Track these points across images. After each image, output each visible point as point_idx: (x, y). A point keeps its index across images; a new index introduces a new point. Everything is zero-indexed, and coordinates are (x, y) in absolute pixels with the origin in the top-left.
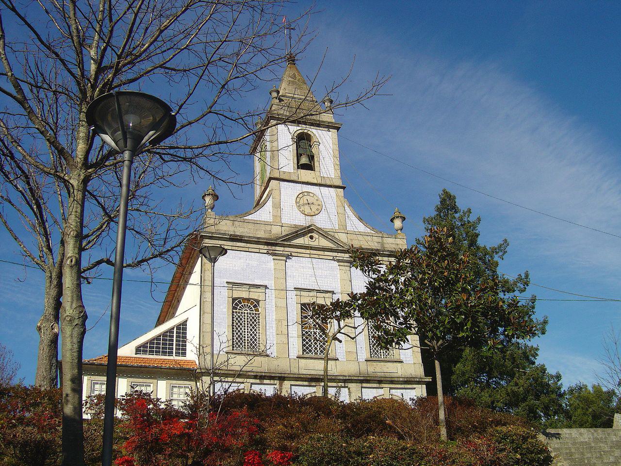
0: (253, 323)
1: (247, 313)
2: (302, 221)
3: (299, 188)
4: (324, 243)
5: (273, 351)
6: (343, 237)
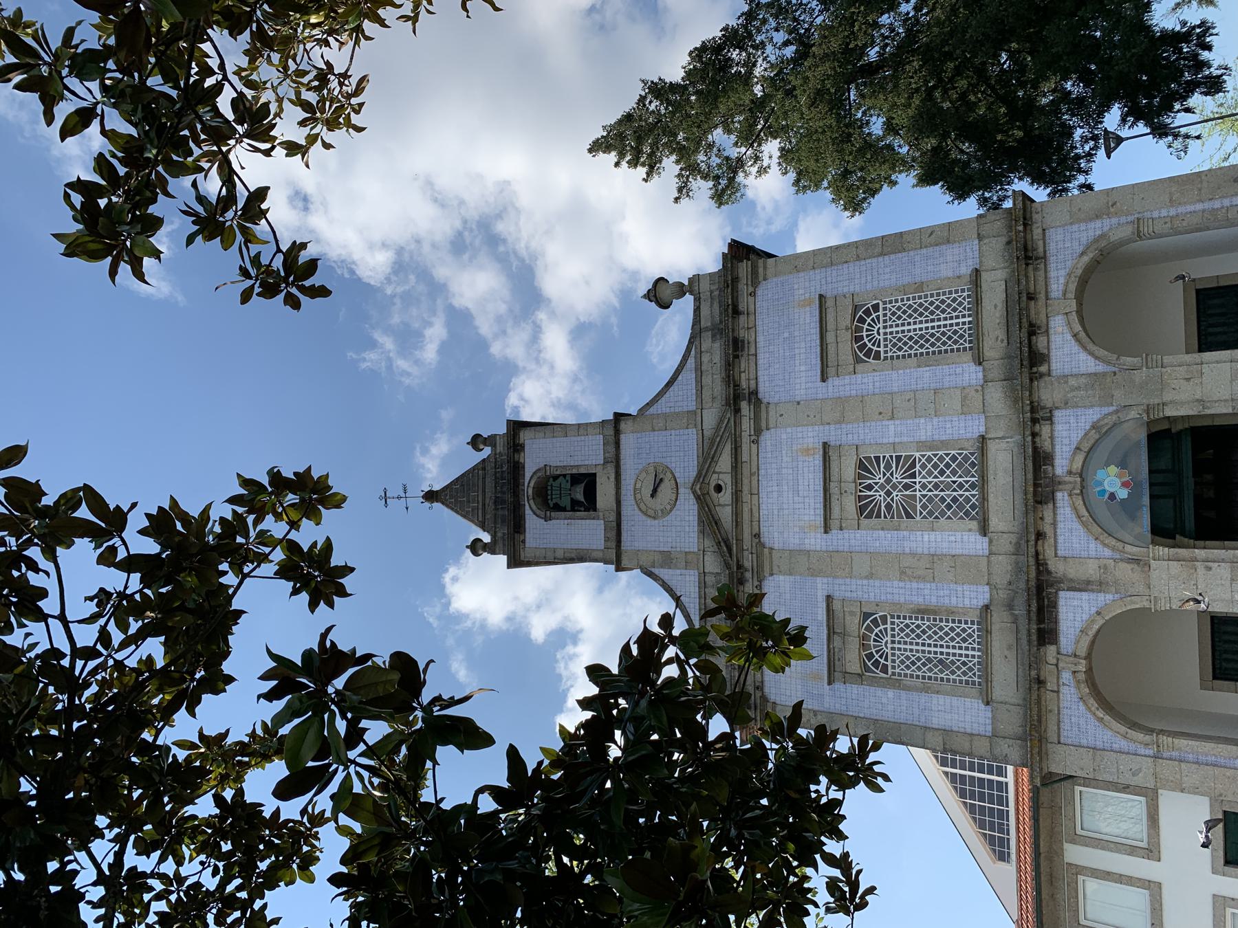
1: (893, 642)
2: (688, 509)
6: (710, 418)
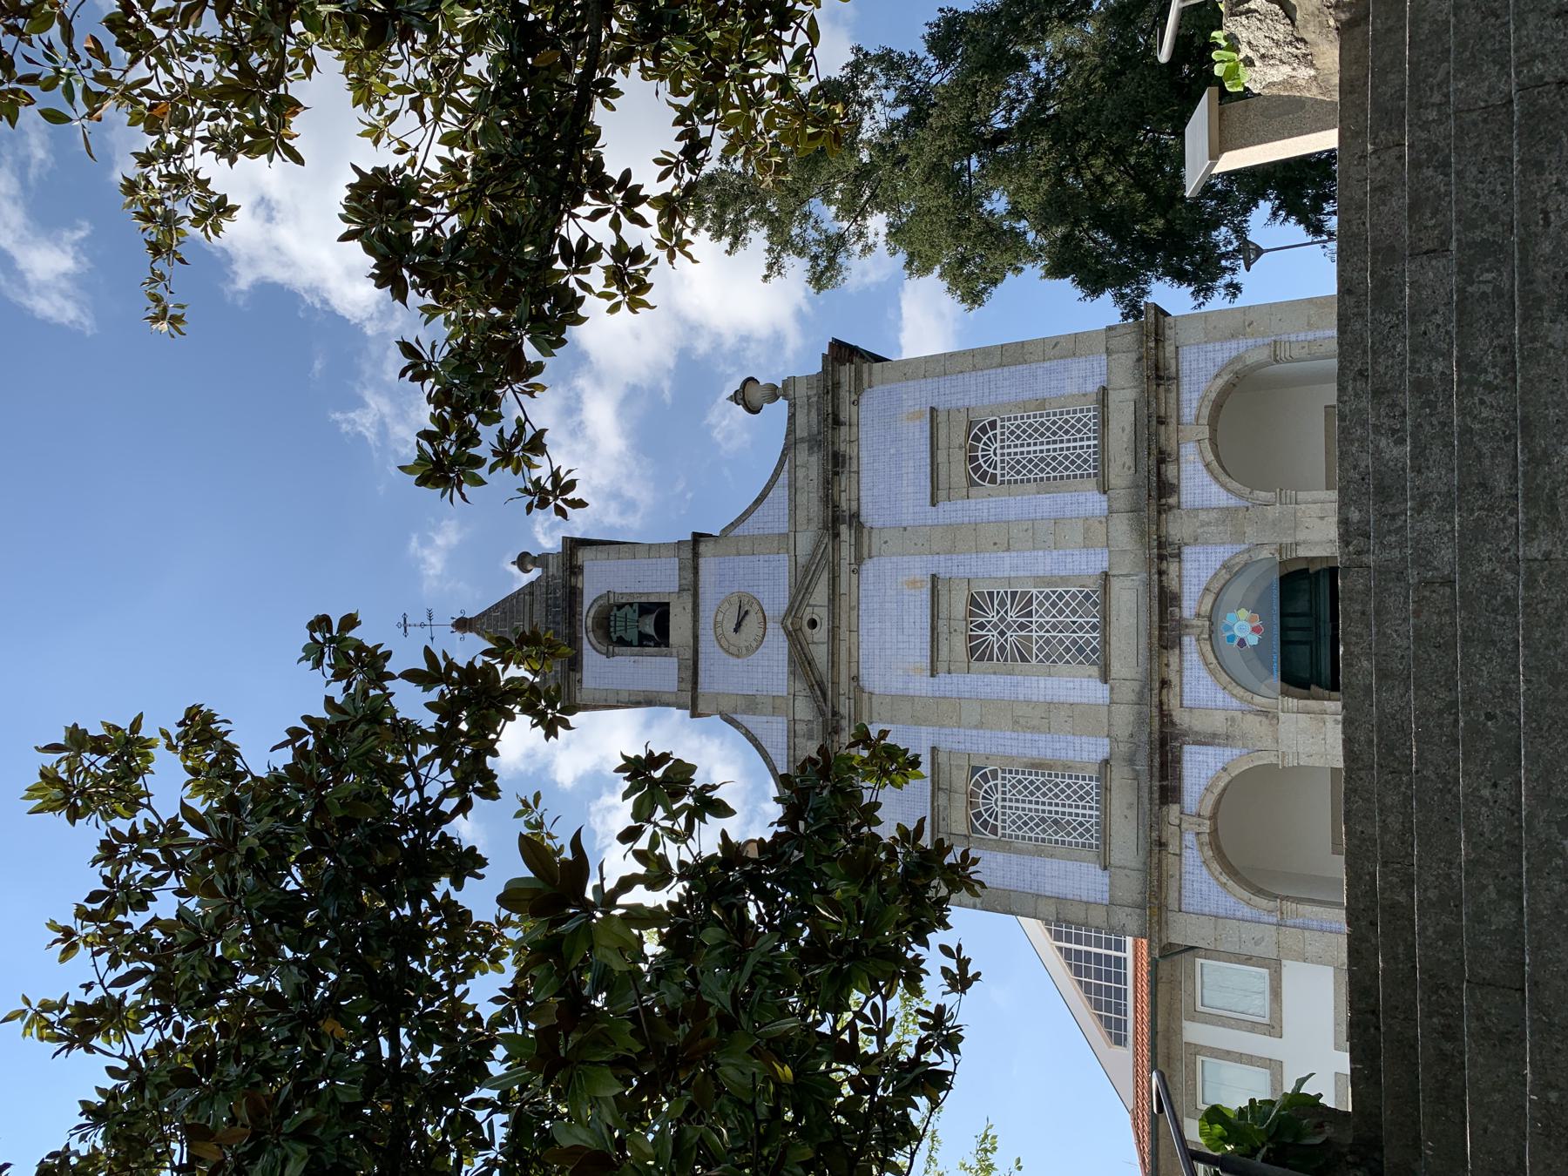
0: (1024, 467)
2: (777, 647)
3: (708, 645)
4: (820, 594)
5: (1096, 562)
